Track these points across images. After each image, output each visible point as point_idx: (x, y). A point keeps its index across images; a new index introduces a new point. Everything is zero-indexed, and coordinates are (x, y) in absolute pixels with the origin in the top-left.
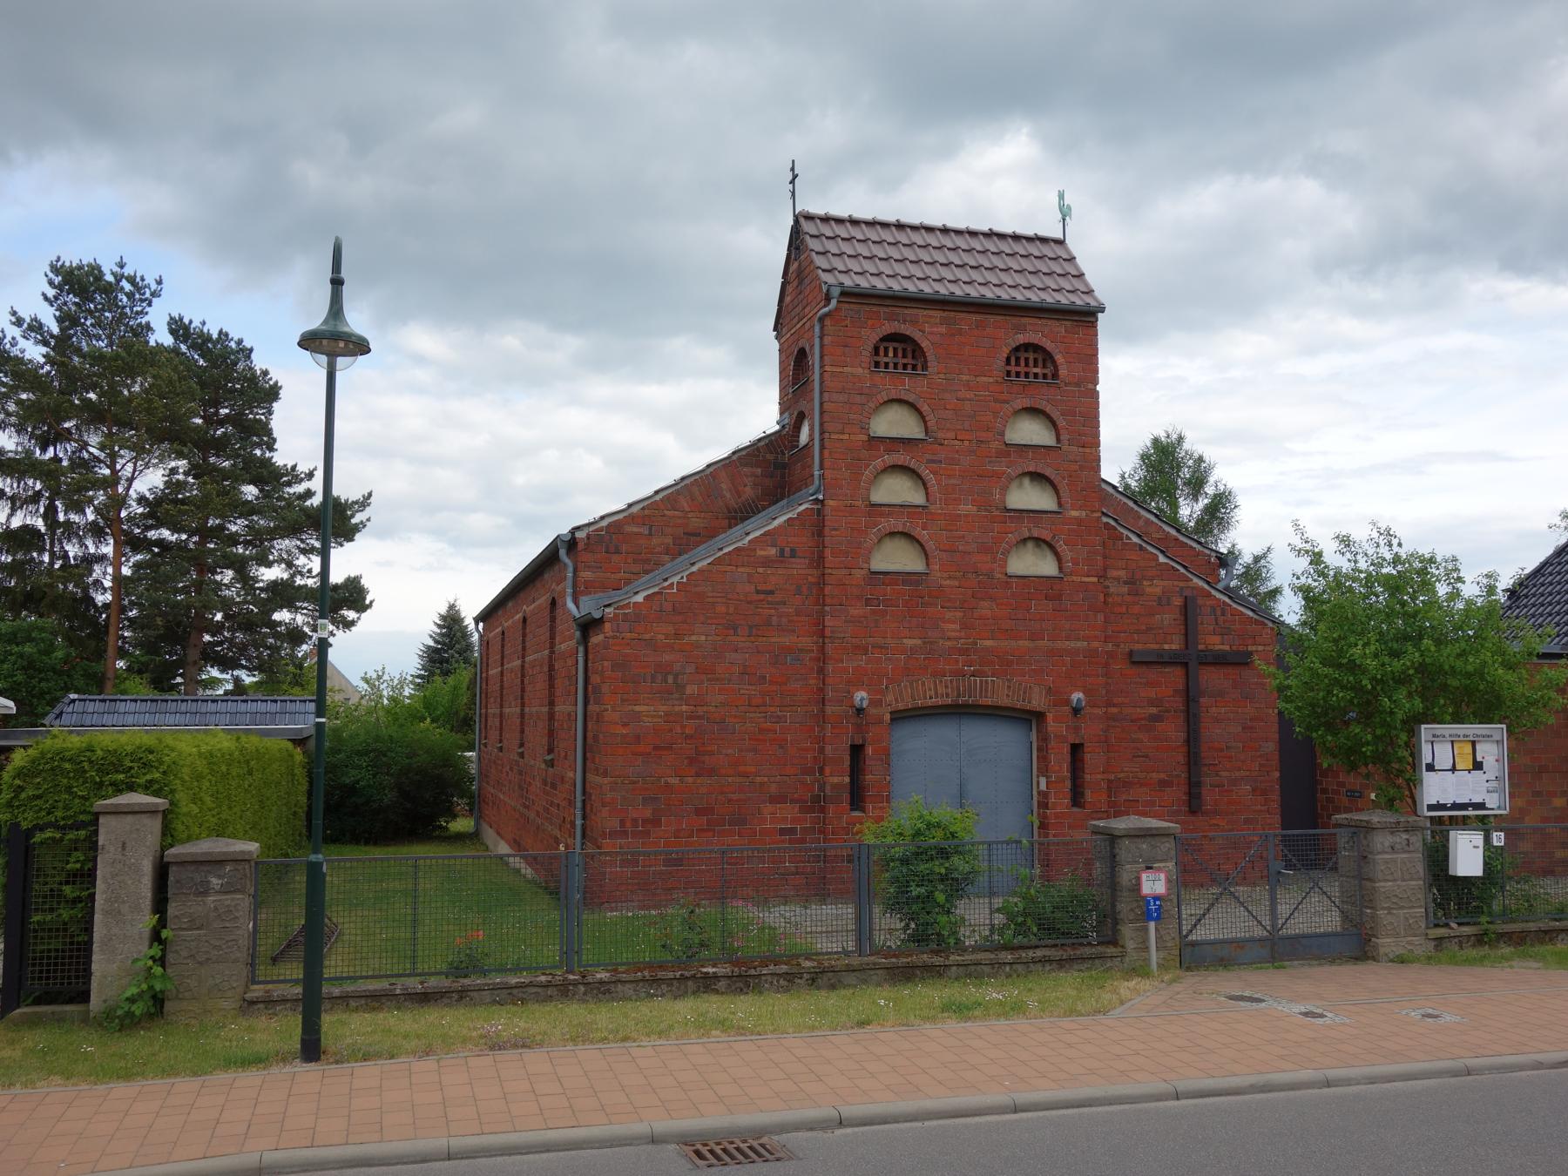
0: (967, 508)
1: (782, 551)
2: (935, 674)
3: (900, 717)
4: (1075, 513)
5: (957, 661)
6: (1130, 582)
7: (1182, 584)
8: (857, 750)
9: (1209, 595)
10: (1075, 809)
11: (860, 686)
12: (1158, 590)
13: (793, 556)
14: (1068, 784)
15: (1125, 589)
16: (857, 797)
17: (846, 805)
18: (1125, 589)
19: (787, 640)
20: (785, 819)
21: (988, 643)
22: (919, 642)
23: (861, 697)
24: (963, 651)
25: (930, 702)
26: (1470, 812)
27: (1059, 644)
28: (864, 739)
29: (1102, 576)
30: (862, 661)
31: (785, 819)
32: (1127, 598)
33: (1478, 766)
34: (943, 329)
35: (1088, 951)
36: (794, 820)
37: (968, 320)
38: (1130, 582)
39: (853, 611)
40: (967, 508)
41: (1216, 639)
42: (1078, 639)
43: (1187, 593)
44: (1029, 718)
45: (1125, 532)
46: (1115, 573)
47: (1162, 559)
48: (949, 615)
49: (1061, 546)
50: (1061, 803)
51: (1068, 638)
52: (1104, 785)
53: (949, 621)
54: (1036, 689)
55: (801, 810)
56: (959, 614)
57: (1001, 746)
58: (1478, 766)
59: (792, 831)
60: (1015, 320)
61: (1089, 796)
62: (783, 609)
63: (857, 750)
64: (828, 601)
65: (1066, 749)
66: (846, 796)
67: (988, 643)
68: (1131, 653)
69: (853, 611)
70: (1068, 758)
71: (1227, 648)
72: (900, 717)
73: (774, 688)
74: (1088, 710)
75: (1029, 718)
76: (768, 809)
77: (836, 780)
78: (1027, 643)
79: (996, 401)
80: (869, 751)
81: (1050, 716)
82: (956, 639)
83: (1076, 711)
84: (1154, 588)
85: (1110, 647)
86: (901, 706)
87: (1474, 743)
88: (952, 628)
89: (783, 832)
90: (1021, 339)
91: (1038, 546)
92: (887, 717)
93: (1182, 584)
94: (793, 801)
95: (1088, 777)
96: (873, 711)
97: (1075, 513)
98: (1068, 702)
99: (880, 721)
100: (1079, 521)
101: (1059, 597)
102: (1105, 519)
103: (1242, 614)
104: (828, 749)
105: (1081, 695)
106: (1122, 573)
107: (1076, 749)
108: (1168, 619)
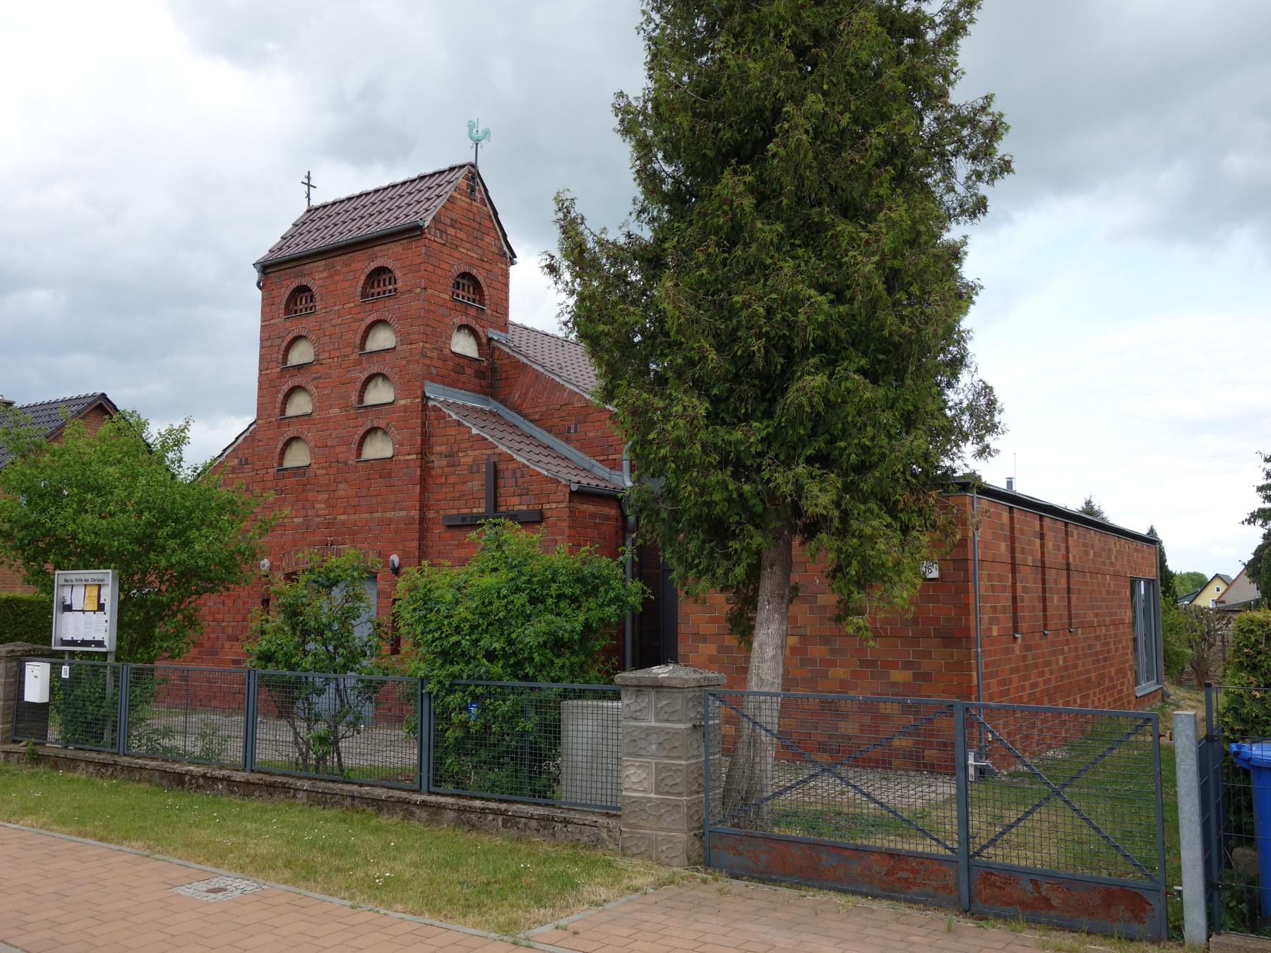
7: (489, 452)
9: (512, 459)
12: (470, 460)
15: (444, 462)
18: (444, 462)
21: (343, 517)
26: (93, 649)
27: (388, 515)
32: (447, 470)
33: (101, 607)
34: (325, 274)
35: (522, 799)
37: (338, 262)
40: (335, 411)
41: (516, 500)
42: (401, 510)
43: (494, 459)
51: (394, 509)
58: (101, 607)
60: (370, 251)
67: (343, 517)
71: (525, 508)
76: (227, 645)
79: (355, 320)
82: (324, 516)
84: (466, 459)
87: (100, 587)
90: (373, 266)
93: (489, 452)
100: (405, 407)
101: (389, 475)
103: (539, 474)
108: (477, 485)
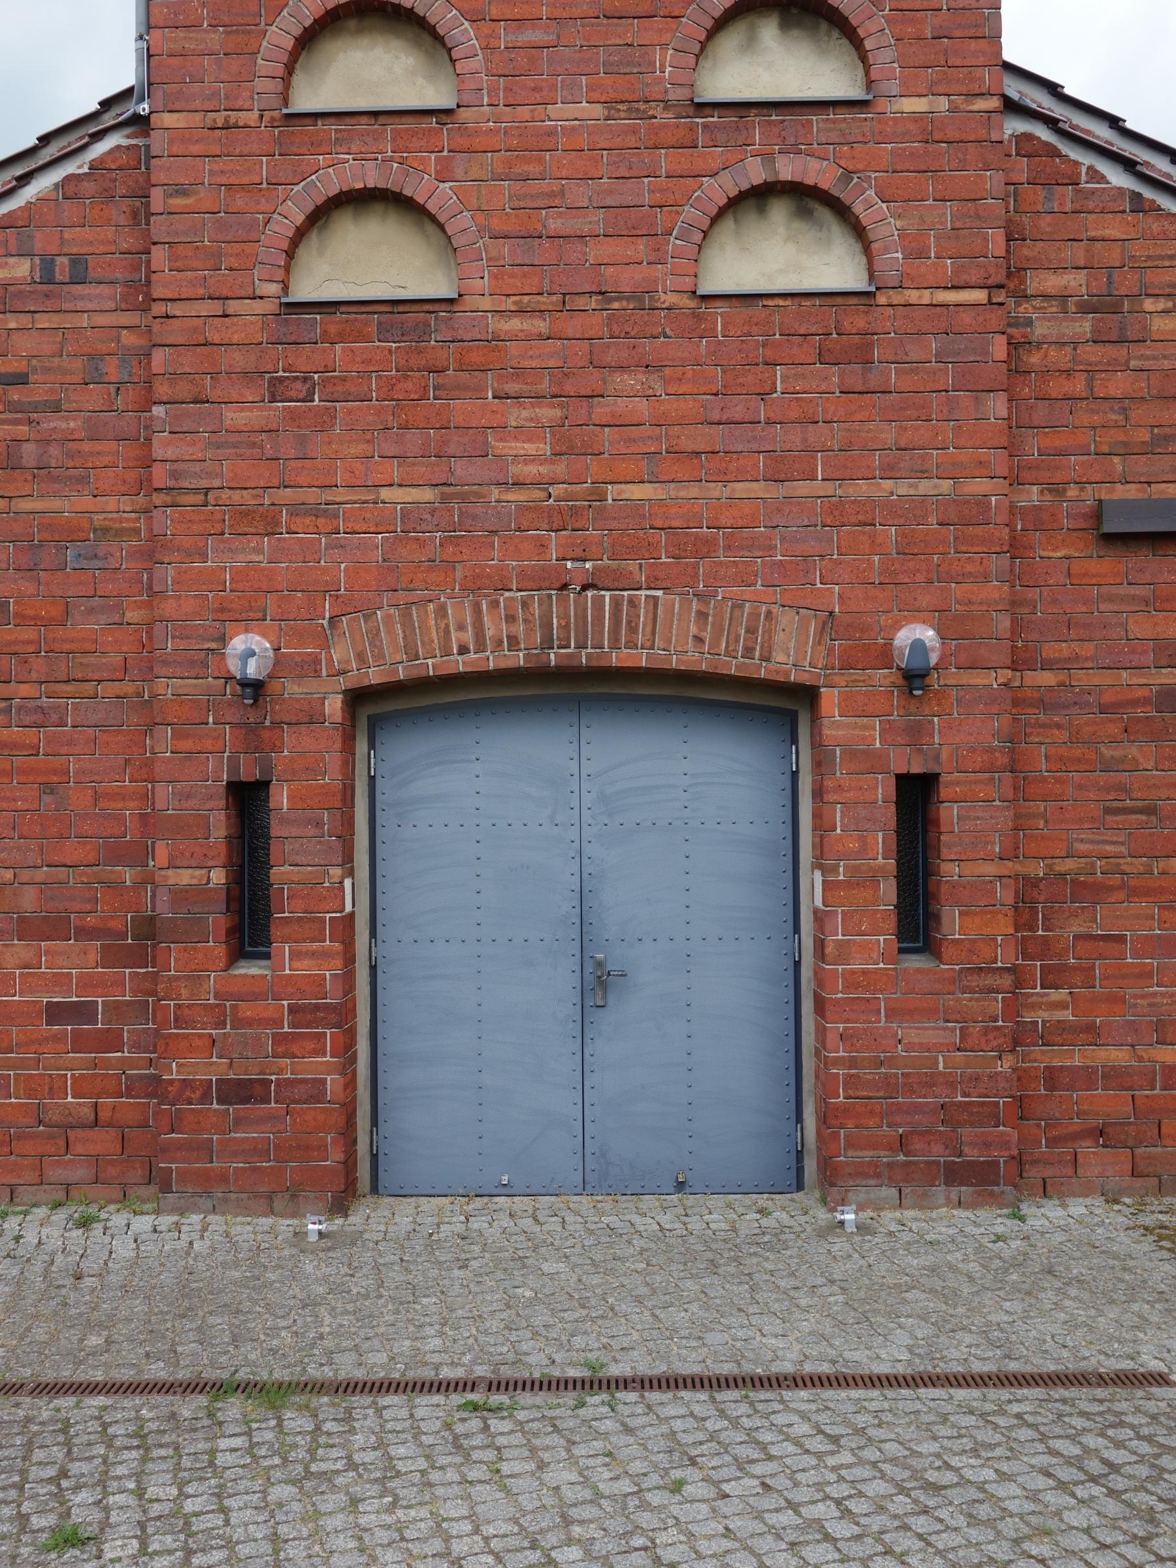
0: (574, 111)
1: (48, 265)
2: (474, 586)
3: (379, 706)
4: (911, 105)
5: (543, 546)
6: (1100, 305)
8: (247, 798)
10: (915, 962)
11: (249, 619)
13: (78, 279)
14: (888, 890)
15: (1085, 326)
16: (250, 919)
17: (216, 948)
19: (65, 505)
20: (61, 981)
22: (427, 495)
23: (249, 651)
24: (563, 519)
25: (461, 664)
27: (861, 489)
28: (268, 769)
29: (1009, 282)
30: (256, 553)
31: (61, 981)
32: (1093, 354)
36: (87, 984)
38: (1100, 305)
39: (234, 417)
40: (574, 111)
42: (922, 474)
44: (779, 706)
45: (1086, 159)
46: (1052, 282)
47: (957, 967)
48: (516, 416)
49: (867, 204)
50: (869, 942)
51: (890, 471)
52: (1004, 894)
53: (520, 433)
54: (787, 619)
55: (111, 957)
56: (549, 413)
57: (710, 778)
59: (83, 1012)
61: (953, 924)
62: (53, 423)
63: (247, 798)
64: (162, 390)
65: (883, 790)
66: (216, 920)
68: (1098, 513)
69: (234, 417)
70: (888, 815)
72: (379, 706)
73: (29, 633)
74: (953, 677)
75: (779, 706)
77: (186, 877)
78: (758, 489)
80: (281, 798)
81: (830, 699)
83: (914, 679)
85: (1033, 495)
86: (374, 676)
88: (527, 455)
89: (56, 1013)
91: (804, 213)
92: (334, 706)
94: (84, 933)
95: (950, 871)
96: (293, 689)
97: (911, 105)
98: (885, 656)
99: (313, 717)
100: (927, 130)
102: (1015, 126)
104: (164, 793)
105: (928, 635)
106: (1074, 281)
107: (916, 795)
